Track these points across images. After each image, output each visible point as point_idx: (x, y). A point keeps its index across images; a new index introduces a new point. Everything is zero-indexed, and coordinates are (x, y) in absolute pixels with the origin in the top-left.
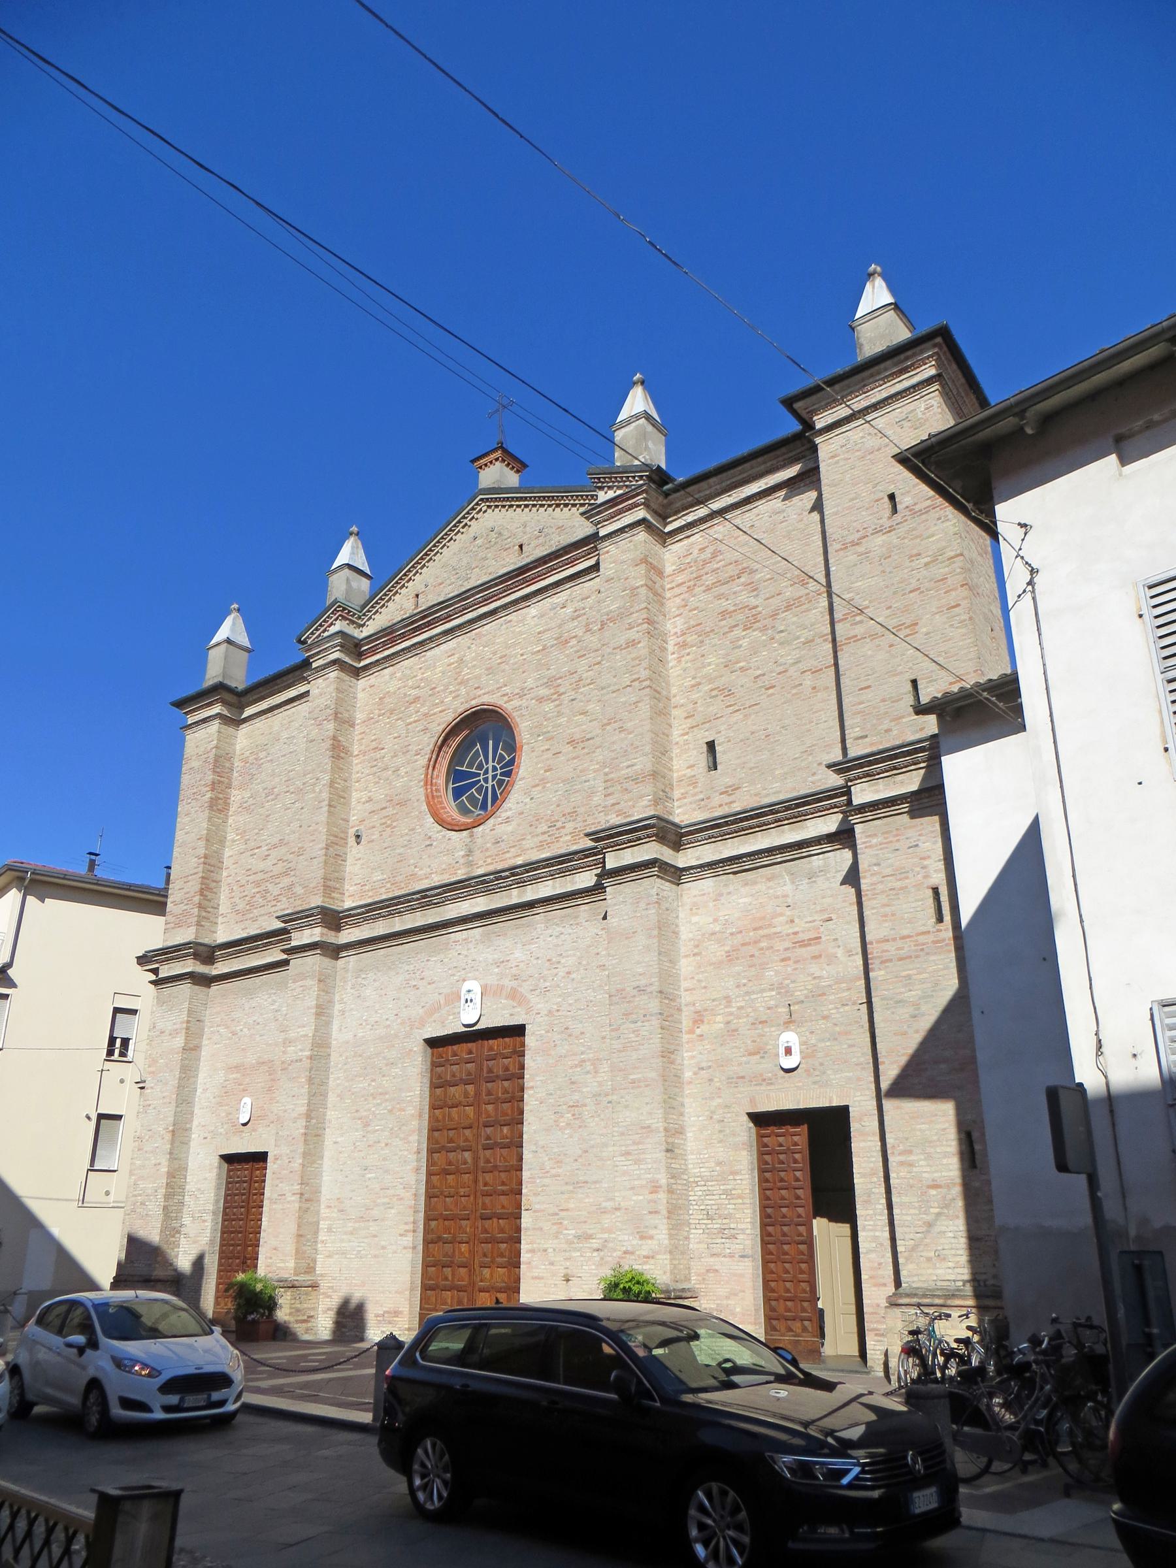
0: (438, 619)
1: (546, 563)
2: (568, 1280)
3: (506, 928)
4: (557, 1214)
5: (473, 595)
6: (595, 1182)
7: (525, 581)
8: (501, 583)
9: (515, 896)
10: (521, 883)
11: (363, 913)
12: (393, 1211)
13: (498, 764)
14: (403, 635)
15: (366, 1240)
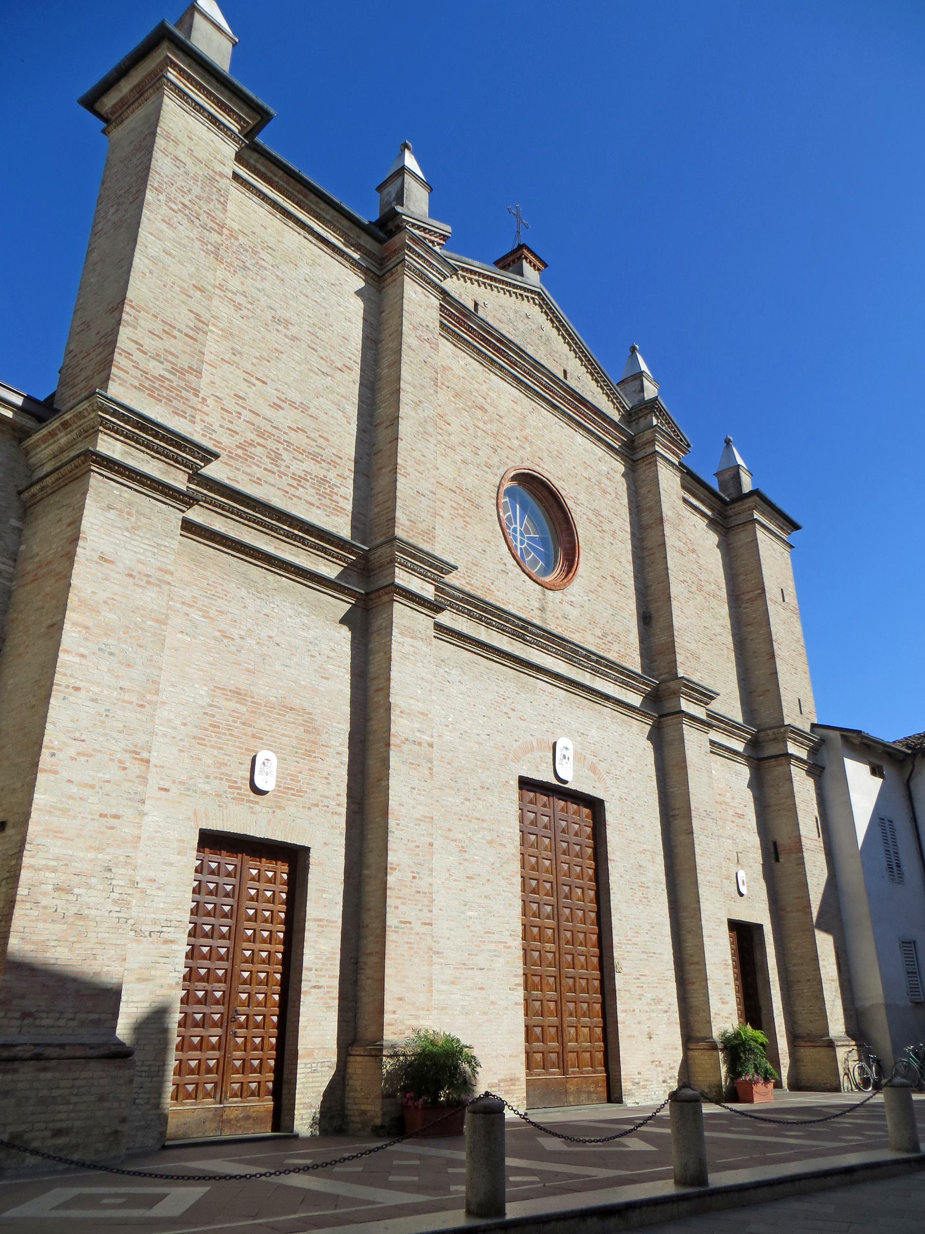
0: (507, 356)
1: (595, 414)
2: (650, 1038)
3: (580, 702)
4: (639, 979)
5: (543, 374)
6: (660, 954)
7: (576, 408)
8: (565, 391)
9: (586, 678)
10: (595, 671)
11: (457, 599)
12: (501, 960)
13: (512, 525)
14: (470, 329)
15: (470, 993)
